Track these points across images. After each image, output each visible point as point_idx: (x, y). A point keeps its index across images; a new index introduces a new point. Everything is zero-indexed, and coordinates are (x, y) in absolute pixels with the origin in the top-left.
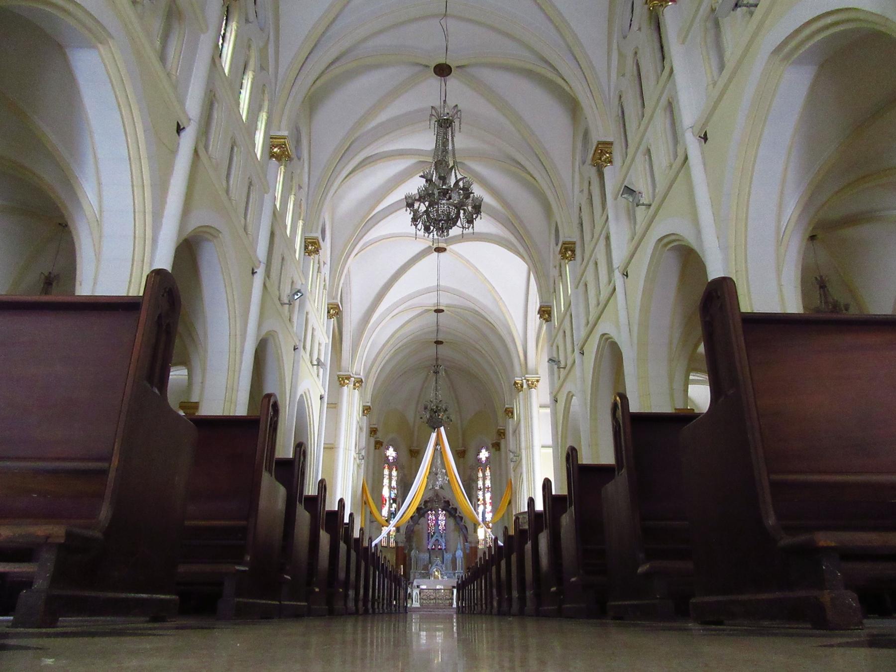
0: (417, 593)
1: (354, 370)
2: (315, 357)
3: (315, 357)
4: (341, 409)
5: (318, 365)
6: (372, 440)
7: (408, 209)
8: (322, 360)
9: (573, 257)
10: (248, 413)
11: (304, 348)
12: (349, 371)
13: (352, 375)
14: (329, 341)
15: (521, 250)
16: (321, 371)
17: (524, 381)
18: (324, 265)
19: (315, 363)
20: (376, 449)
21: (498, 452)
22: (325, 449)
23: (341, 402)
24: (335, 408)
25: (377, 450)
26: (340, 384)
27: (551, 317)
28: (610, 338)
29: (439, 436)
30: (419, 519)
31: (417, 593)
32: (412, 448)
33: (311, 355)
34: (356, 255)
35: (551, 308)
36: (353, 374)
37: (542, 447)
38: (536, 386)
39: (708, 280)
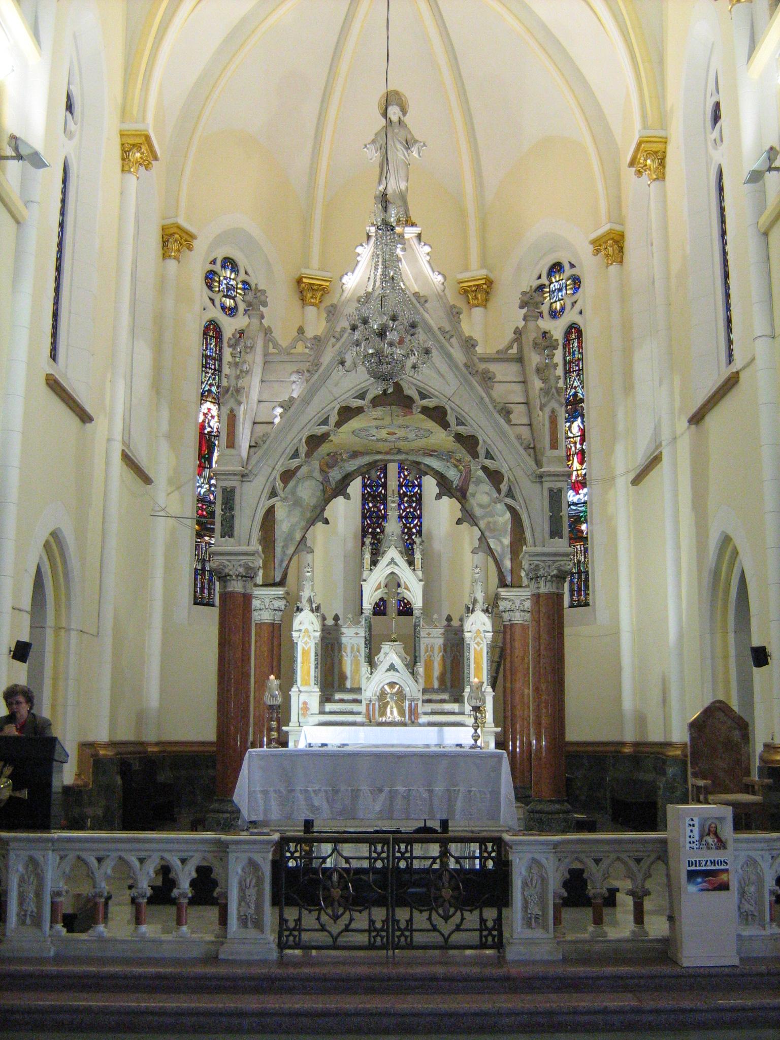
20: (165, 256)
21: (614, 268)
25: (172, 264)
32: (305, 271)
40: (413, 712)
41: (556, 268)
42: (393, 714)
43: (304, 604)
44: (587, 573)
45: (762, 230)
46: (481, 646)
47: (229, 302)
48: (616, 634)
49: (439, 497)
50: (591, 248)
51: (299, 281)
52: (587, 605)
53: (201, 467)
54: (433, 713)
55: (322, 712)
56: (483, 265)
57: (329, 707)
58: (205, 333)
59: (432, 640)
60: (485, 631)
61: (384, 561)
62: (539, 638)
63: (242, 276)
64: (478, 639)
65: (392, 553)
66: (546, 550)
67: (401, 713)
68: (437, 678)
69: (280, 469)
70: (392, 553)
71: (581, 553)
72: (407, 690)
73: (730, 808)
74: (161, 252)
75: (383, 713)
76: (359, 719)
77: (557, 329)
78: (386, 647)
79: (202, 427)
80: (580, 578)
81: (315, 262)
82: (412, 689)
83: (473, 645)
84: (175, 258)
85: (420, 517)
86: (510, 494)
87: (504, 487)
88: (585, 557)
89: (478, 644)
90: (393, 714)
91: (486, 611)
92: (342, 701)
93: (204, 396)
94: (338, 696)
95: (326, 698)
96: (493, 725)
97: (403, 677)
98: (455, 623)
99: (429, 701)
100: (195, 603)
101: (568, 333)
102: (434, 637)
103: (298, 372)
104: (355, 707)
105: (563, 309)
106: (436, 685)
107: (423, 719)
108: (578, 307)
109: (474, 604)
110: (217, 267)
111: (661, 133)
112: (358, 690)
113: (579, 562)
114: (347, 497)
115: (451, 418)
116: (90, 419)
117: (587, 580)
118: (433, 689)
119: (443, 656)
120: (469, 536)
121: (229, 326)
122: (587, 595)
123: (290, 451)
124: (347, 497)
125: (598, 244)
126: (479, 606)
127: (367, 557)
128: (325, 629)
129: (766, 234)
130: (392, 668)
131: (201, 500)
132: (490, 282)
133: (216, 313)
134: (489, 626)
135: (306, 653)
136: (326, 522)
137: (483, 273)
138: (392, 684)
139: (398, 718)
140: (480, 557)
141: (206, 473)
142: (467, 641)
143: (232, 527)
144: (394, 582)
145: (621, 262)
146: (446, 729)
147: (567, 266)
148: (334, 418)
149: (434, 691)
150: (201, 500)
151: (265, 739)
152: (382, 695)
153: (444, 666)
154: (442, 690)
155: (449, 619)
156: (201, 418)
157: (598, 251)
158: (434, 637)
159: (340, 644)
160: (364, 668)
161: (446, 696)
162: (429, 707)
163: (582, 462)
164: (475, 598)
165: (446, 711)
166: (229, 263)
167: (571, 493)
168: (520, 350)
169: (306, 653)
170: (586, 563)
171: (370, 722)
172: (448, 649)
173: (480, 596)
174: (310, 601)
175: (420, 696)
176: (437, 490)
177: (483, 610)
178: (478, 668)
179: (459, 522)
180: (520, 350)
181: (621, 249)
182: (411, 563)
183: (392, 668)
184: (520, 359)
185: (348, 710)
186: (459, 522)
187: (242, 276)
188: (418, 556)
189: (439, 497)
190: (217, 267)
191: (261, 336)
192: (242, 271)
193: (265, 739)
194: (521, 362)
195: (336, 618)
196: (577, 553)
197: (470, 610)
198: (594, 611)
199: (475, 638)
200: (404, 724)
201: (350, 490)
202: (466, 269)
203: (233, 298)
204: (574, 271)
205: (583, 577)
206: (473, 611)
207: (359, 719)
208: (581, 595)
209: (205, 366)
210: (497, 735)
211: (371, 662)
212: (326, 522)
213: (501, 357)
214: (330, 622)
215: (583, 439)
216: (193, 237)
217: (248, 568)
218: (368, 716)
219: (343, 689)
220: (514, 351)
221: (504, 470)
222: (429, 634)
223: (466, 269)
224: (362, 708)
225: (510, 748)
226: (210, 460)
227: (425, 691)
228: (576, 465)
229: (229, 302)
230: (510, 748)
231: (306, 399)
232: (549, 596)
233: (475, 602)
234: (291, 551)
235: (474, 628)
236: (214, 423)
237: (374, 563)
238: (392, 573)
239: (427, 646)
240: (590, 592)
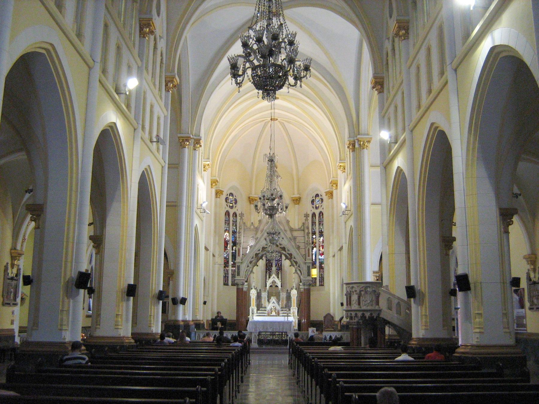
0: (255, 335)
1: (194, 133)
2: (155, 134)
3: (155, 134)
4: (183, 169)
5: (158, 142)
6: (214, 191)
7: (233, 79)
8: (161, 136)
9: (406, 36)
10: (79, 291)
11: (143, 128)
12: (188, 134)
13: (191, 136)
14: (168, 113)
15: (357, 21)
16: (161, 147)
17: (356, 141)
18: (160, 39)
19: (155, 140)
20: (216, 197)
21: (330, 200)
22: (168, 207)
23: (183, 163)
24: (177, 168)
25: (218, 199)
26: (181, 146)
27: (383, 88)
28: (438, 127)
29: (291, 66)
30: (258, 261)
31: (255, 335)
32: (251, 195)
33: (150, 133)
34: (193, 24)
35: (383, 79)
36: (192, 135)
37: (372, 204)
38: (367, 146)
39: (522, 219)
40: (278, 312)
41: (317, 195)
42: (274, 313)
43: (253, 287)
45: (454, 68)
47: (231, 205)
49: (285, 260)
50: (325, 194)
51: (249, 198)
53: (225, 250)
54: (283, 313)
55: (257, 313)
56: (298, 194)
57: (259, 312)
58: (225, 214)
61: (272, 277)
63: (234, 197)
65: (274, 275)
66: (306, 279)
67: (276, 313)
69: (249, 261)
70: (274, 275)
72: (277, 308)
73: (235, 318)
74: (215, 196)
75: (271, 313)
76: (266, 315)
77: (317, 212)
78: (272, 298)
79: (225, 239)
81: (253, 192)
82: (278, 308)
83: (293, 297)
84: (219, 198)
85: (281, 261)
86: (299, 266)
87: (298, 265)
90: (274, 313)
91: (296, 289)
92: (262, 310)
93: (225, 231)
94: (261, 309)
95: (258, 310)
97: (276, 304)
98: (289, 291)
99: (282, 310)
100: (224, 285)
101: (320, 214)
103: (252, 237)
104: (265, 312)
105: (319, 206)
107: (281, 315)
108: (322, 207)
110: (228, 196)
111: (407, 18)
112: (266, 308)
114: (263, 260)
115: (286, 250)
116: (208, 250)
120: (293, 269)
121: (232, 212)
123: (251, 257)
124: (263, 260)
125: (327, 193)
126: (294, 288)
127: (268, 276)
128: (258, 293)
129: (346, 223)
130: (274, 303)
131: (225, 258)
132: (300, 198)
133: (228, 209)
134: (296, 293)
135: (253, 299)
136: (258, 266)
137: (298, 196)
138: (273, 307)
139: (275, 315)
140: (296, 275)
141: (226, 251)
143: (239, 274)
144: (274, 282)
145: (332, 198)
147: (320, 196)
148: (261, 249)
150: (225, 258)
152: (271, 309)
154: (286, 307)
155: (287, 290)
156: (225, 237)
157: (326, 195)
159: (261, 297)
160: (267, 303)
162: (282, 312)
163: (323, 248)
166: (231, 194)
167: (320, 256)
168: (304, 228)
169: (253, 299)
171: (269, 315)
173: (294, 285)
174: (254, 287)
175: (280, 309)
176: (285, 258)
178: (294, 303)
179: (290, 266)
180: (304, 228)
181: (332, 195)
182: (278, 277)
183: (274, 303)
184: (304, 230)
185: (74, 42)
186: (290, 266)
187: (234, 197)
188: (280, 276)
189: (285, 260)
190: (228, 196)
191: (243, 224)
192: (234, 196)
195: (260, 290)
197: (292, 289)
200: (276, 316)
201: (263, 258)
202: (294, 194)
203: (232, 204)
204: (321, 197)
207: (266, 315)
209: (226, 223)
210: (298, 318)
211: (269, 301)
212: (258, 266)
213: (299, 230)
214: (259, 291)
215: (323, 243)
216: (223, 191)
217: (242, 282)
218: (268, 314)
219: (262, 307)
220: (302, 228)
221: (298, 261)
223: (294, 194)
224: (267, 312)
226: (227, 247)
227: (281, 308)
228: (321, 249)
229: (231, 205)
231: (255, 246)
232: (307, 289)
233: (293, 287)
234: (249, 273)
236: (228, 238)
237: (269, 277)
238: (274, 280)
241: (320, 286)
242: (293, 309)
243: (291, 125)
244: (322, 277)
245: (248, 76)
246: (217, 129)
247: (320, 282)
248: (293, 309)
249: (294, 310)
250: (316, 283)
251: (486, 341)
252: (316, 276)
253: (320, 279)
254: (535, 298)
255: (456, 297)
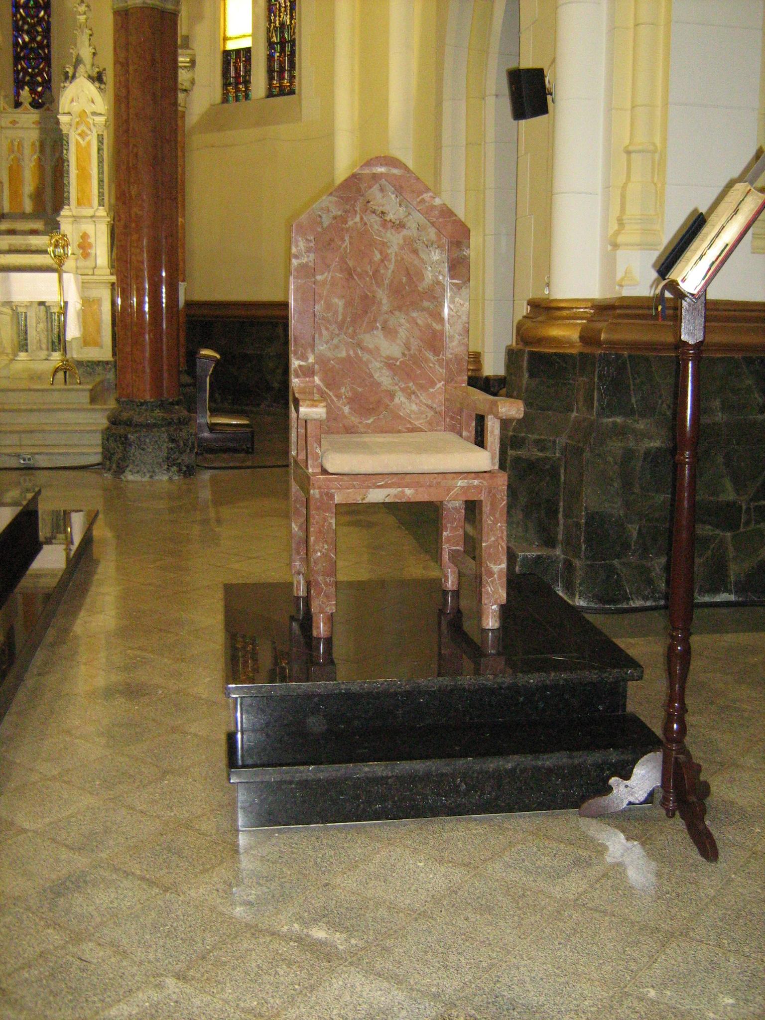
44: (293, 43)
46: (88, 139)
48: (329, 135)
52: (292, 92)
54: (11, 251)
59: (20, 134)
60: (94, 114)
62: (127, 97)
64: (83, 128)
68: (30, 196)
71: (285, 11)
80: (283, 50)
83: (74, 138)
88: (292, 18)
89: (83, 135)
96: (108, 271)
102: (22, 128)
106: (28, 207)
109: (75, 68)
113: (282, 24)
117: (293, 53)
118: (24, 213)
119: (39, 159)
122: (292, 77)
142: (65, 130)
146: (15, 276)
149: (23, 216)
151: (164, 326)
153: (42, 178)
154: (36, 215)
158: (22, 128)
161: (38, 225)
164: (78, 56)
165: (33, 248)
170: (292, 28)
172: (48, 150)
177: (91, 78)
178: (84, 175)
193: (164, 326)
194: (548, 286)
196: (280, 12)
198: (300, 100)
199: (78, 123)
205: (288, 49)
206: (74, 77)
208: (284, 78)
222: (14, 122)
225: (690, 365)
230: (690, 365)
235: (76, 108)
239: (12, 142)
240: (296, 73)
241: (270, 95)
242: (76, 219)
243: (575, 310)
244: (283, 43)
245: (596, 611)
246: (631, 62)
247: (270, 71)
248: (76, 219)
249: (88, 227)
250: (247, 83)
251: (535, 297)
252: (247, 43)
253: (270, 58)
254: (721, 996)
255: (513, 65)
